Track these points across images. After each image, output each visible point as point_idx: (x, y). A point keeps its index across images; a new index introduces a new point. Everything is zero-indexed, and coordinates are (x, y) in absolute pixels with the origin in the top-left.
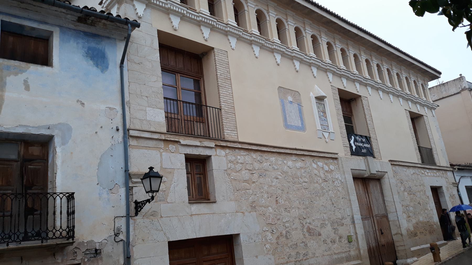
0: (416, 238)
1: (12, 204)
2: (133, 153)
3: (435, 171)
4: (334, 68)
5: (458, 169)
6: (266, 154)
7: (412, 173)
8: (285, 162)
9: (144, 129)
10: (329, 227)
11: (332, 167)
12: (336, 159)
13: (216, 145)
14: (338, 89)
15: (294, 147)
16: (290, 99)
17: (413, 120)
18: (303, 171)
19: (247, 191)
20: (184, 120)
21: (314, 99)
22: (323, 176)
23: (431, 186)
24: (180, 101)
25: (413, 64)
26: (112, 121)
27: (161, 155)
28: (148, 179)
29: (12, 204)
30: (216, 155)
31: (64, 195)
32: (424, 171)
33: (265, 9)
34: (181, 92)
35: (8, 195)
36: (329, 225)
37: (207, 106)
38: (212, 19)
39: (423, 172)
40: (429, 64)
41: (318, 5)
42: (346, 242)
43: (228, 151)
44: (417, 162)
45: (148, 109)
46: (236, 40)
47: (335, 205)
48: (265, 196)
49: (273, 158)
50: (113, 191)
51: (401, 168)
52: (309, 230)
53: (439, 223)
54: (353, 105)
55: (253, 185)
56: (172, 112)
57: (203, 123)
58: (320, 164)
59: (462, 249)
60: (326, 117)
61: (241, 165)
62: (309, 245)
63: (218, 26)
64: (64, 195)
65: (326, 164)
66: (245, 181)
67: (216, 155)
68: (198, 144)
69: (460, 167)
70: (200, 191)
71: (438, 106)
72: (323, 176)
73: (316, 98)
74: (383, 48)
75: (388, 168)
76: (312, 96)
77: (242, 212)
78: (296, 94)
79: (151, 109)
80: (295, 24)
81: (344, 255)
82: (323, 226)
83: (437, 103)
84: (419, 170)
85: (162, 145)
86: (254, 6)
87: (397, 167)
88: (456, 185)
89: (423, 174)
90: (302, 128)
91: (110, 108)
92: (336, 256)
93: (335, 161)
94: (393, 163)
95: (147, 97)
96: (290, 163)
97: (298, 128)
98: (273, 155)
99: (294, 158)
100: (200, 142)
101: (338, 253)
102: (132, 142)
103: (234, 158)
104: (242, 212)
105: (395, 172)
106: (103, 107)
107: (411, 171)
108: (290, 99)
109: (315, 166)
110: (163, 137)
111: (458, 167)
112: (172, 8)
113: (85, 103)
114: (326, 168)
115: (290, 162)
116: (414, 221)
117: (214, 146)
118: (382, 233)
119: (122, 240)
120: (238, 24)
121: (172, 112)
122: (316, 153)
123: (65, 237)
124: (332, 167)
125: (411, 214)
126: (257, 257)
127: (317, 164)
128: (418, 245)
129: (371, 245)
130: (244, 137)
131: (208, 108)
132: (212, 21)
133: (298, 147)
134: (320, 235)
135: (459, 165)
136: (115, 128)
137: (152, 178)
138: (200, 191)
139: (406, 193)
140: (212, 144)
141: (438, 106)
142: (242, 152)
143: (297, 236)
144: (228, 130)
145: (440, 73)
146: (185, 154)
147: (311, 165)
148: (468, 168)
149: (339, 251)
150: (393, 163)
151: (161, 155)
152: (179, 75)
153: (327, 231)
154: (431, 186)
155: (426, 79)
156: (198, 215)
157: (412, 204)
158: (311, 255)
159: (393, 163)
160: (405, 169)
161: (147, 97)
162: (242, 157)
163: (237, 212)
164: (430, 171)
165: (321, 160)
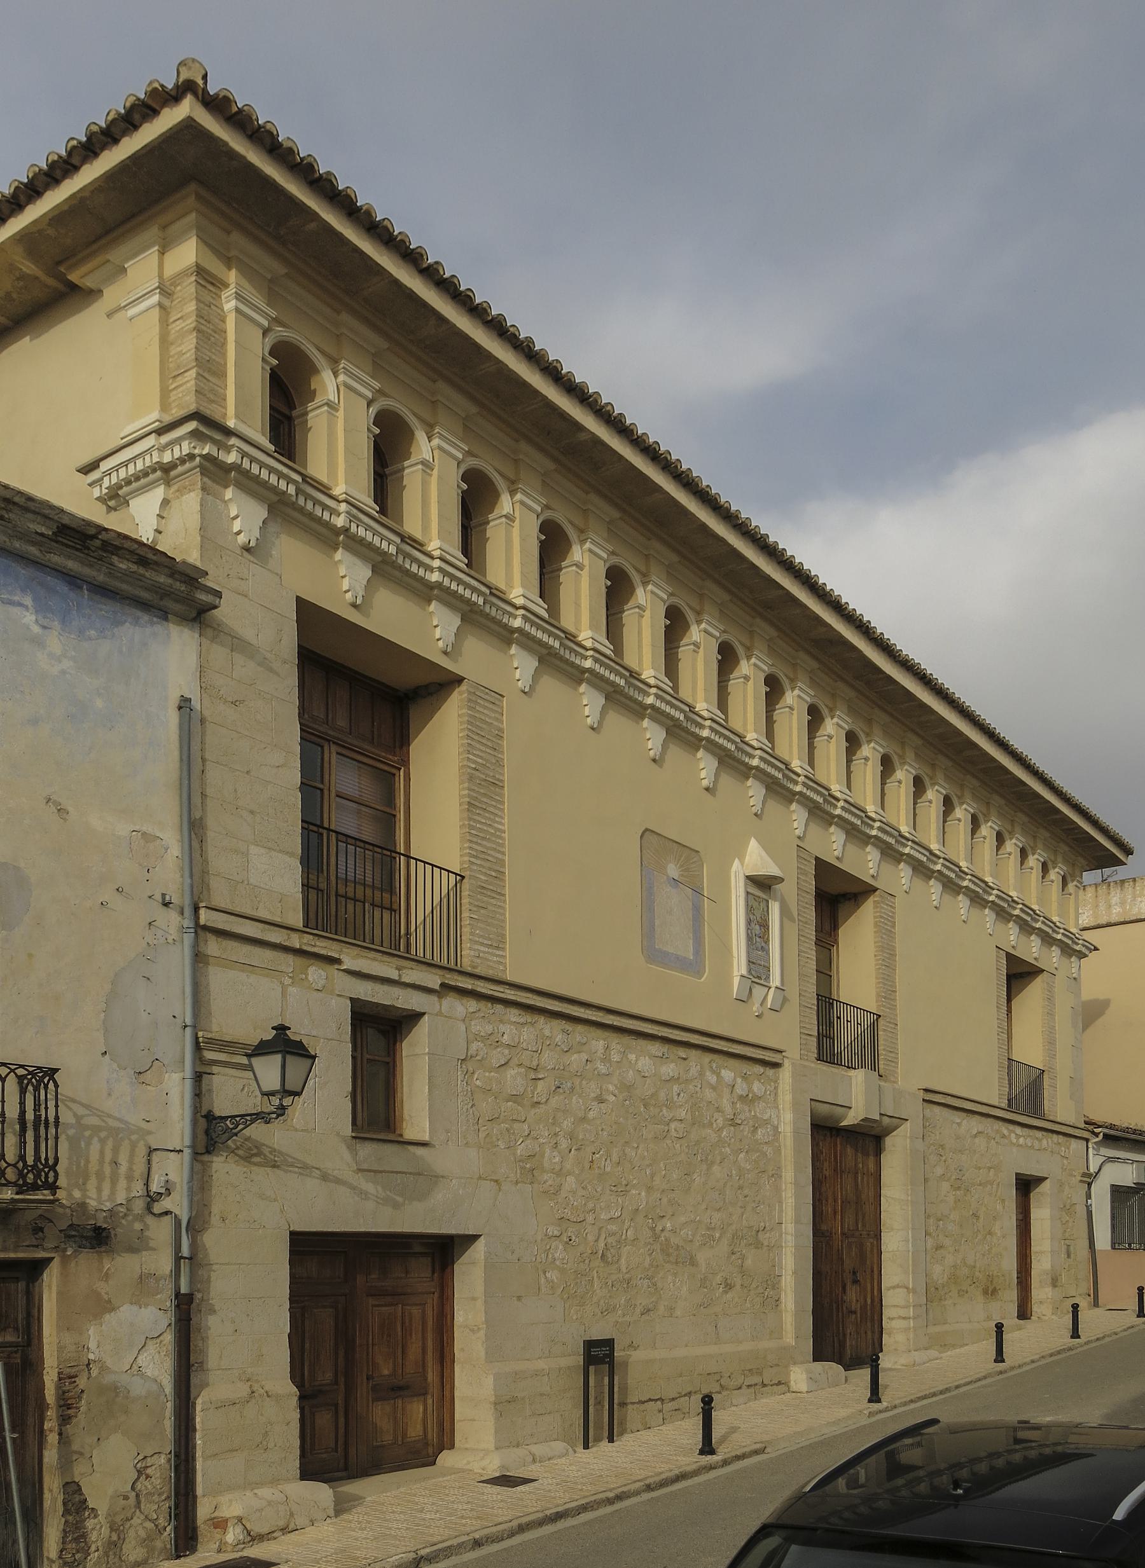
2: (218, 979)
3: (1039, 1134)
4: (729, 740)
5: (1106, 1136)
6: (580, 1028)
7: (975, 1132)
8: (632, 1057)
9: (238, 909)
11: (757, 1087)
12: (776, 1065)
13: (443, 985)
14: (817, 858)
16: (673, 871)
17: (1010, 978)
18: (676, 1088)
19: (516, 1125)
20: (337, 895)
21: (742, 882)
22: (728, 1109)
23: (1017, 1174)
24: (329, 830)
25: (1058, 811)
26: (148, 876)
27: (284, 994)
28: (279, 1057)
30: (440, 1014)
31: (13, 1071)
32: (1011, 1132)
33: (691, 608)
34: (333, 806)
35: (13, 1067)
37: (408, 857)
38: (285, 470)
39: (1006, 1132)
41: (728, 510)
43: (472, 1005)
44: (996, 1104)
45: (254, 850)
46: (369, 573)
48: (564, 1146)
49: (598, 1042)
50: (147, 1077)
51: (946, 1112)
54: (414, 713)
55: (533, 1111)
56: (369, 880)
57: (391, 910)
58: (727, 1075)
59: (696, 1460)
60: (767, 942)
61: (507, 1052)
63: (301, 501)
64: (13, 1071)
65: (745, 1077)
66: (515, 1098)
67: (440, 1014)
68: (393, 974)
69: (1112, 1132)
70: (375, 1110)
71: (1096, 949)
72: (728, 1109)
73: (748, 877)
74: (981, 749)
75: (913, 1108)
76: (738, 872)
77: (496, 1181)
78: (688, 854)
79: (263, 851)
80: (672, 594)
83: (1091, 936)
84: (998, 1125)
85: (288, 962)
86: (605, 556)
87: (937, 1109)
88: (1089, 1179)
89: (1004, 1136)
90: (694, 967)
91: (144, 834)
93: (770, 1072)
94: (932, 1097)
95: (252, 812)
96: (645, 1063)
97: (683, 965)
98: (599, 1032)
99: (656, 1048)
100: (399, 969)
102: (213, 946)
103: (489, 1028)
104: (496, 1181)
105: (926, 1123)
106: (123, 829)
107: (974, 1124)
108: (673, 871)
109: (713, 1079)
110: (295, 941)
111: (1106, 1131)
112: (626, 690)
113: (70, 809)
115: (643, 1059)
117: (437, 987)
119: (167, 1213)
120: (383, 511)
121: (369, 880)
122: (723, 1043)
123: (15, 1184)
124: (757, 1087)
126: (519, 1298)
127: (718, 1075)
130: (517, 965)
131: (413, 862)
132: (281, 476)
134: (693, 1262)
135: (1111, 1127)
136: (159, 897)
137: (288, 1057)
138: (375, 1110)
139: (945, 1186)
140: (433, 980)
141: (1096, 949)
142: (513, 1014)
144: (482, 944)
145: (1128, 852)
146: (351, 999)
147: (701, 1074)
148: (1133, 1136)
150: (930, 1097)
151: (284, 994)
152: (334, 748)
154: (1017, 1174)
155: (1082, 861)
156: (375, 1171)
159: (930, 1097)
160: (957, 1117)
161: (252, 812)
162: (512, 1027)
163: (480, 1178)
164: (1026, 1131)
165: (732, 1062)
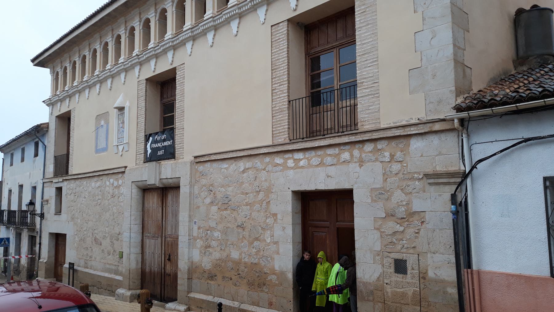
0: (212, 282)
1: (495, 154)
10: (108, 240)
15: (93, 170)
29: (495, 154)
36: (108, 238)
40: (58, 38)
42: (118, 256)
47: (115, 220)
52: (96, 239)
53: (290, 276)
62: (93, 250)
81: (113, 267)
82: (104, 238)
92: (108, 266)
99: (96, 179)
101: (110, 264)
114: (116, 184)
116: (217, 255)
118: (169, 260)
125: (214, 243)
128: (211, 295)
129: (152, 268)
133: (96, 170)
139: (214, 209)
143: (89, 240)
149: (111, 262)
153: (106, 243)
157: (220, 227)
158: (93, 258)
164: (313, 153)
